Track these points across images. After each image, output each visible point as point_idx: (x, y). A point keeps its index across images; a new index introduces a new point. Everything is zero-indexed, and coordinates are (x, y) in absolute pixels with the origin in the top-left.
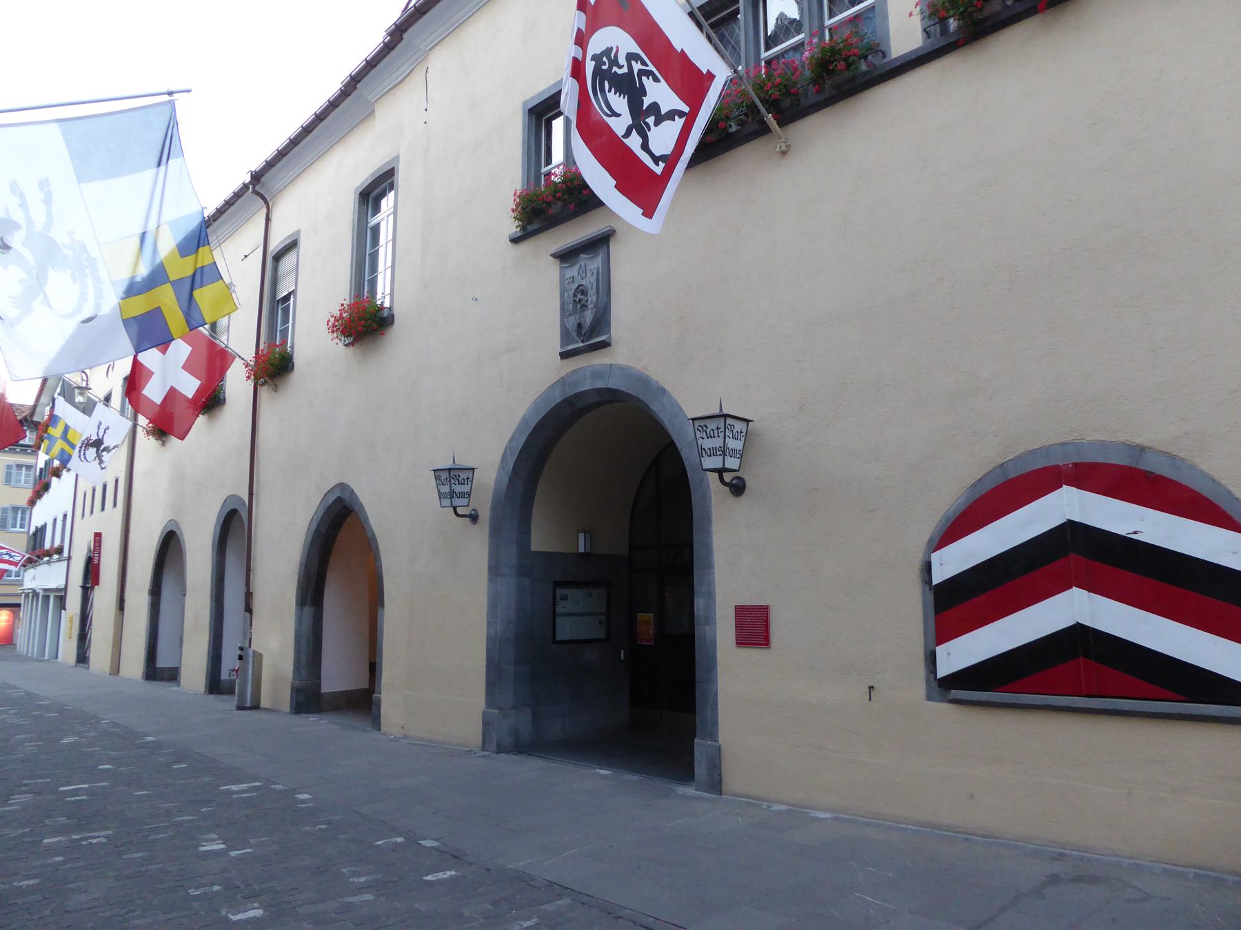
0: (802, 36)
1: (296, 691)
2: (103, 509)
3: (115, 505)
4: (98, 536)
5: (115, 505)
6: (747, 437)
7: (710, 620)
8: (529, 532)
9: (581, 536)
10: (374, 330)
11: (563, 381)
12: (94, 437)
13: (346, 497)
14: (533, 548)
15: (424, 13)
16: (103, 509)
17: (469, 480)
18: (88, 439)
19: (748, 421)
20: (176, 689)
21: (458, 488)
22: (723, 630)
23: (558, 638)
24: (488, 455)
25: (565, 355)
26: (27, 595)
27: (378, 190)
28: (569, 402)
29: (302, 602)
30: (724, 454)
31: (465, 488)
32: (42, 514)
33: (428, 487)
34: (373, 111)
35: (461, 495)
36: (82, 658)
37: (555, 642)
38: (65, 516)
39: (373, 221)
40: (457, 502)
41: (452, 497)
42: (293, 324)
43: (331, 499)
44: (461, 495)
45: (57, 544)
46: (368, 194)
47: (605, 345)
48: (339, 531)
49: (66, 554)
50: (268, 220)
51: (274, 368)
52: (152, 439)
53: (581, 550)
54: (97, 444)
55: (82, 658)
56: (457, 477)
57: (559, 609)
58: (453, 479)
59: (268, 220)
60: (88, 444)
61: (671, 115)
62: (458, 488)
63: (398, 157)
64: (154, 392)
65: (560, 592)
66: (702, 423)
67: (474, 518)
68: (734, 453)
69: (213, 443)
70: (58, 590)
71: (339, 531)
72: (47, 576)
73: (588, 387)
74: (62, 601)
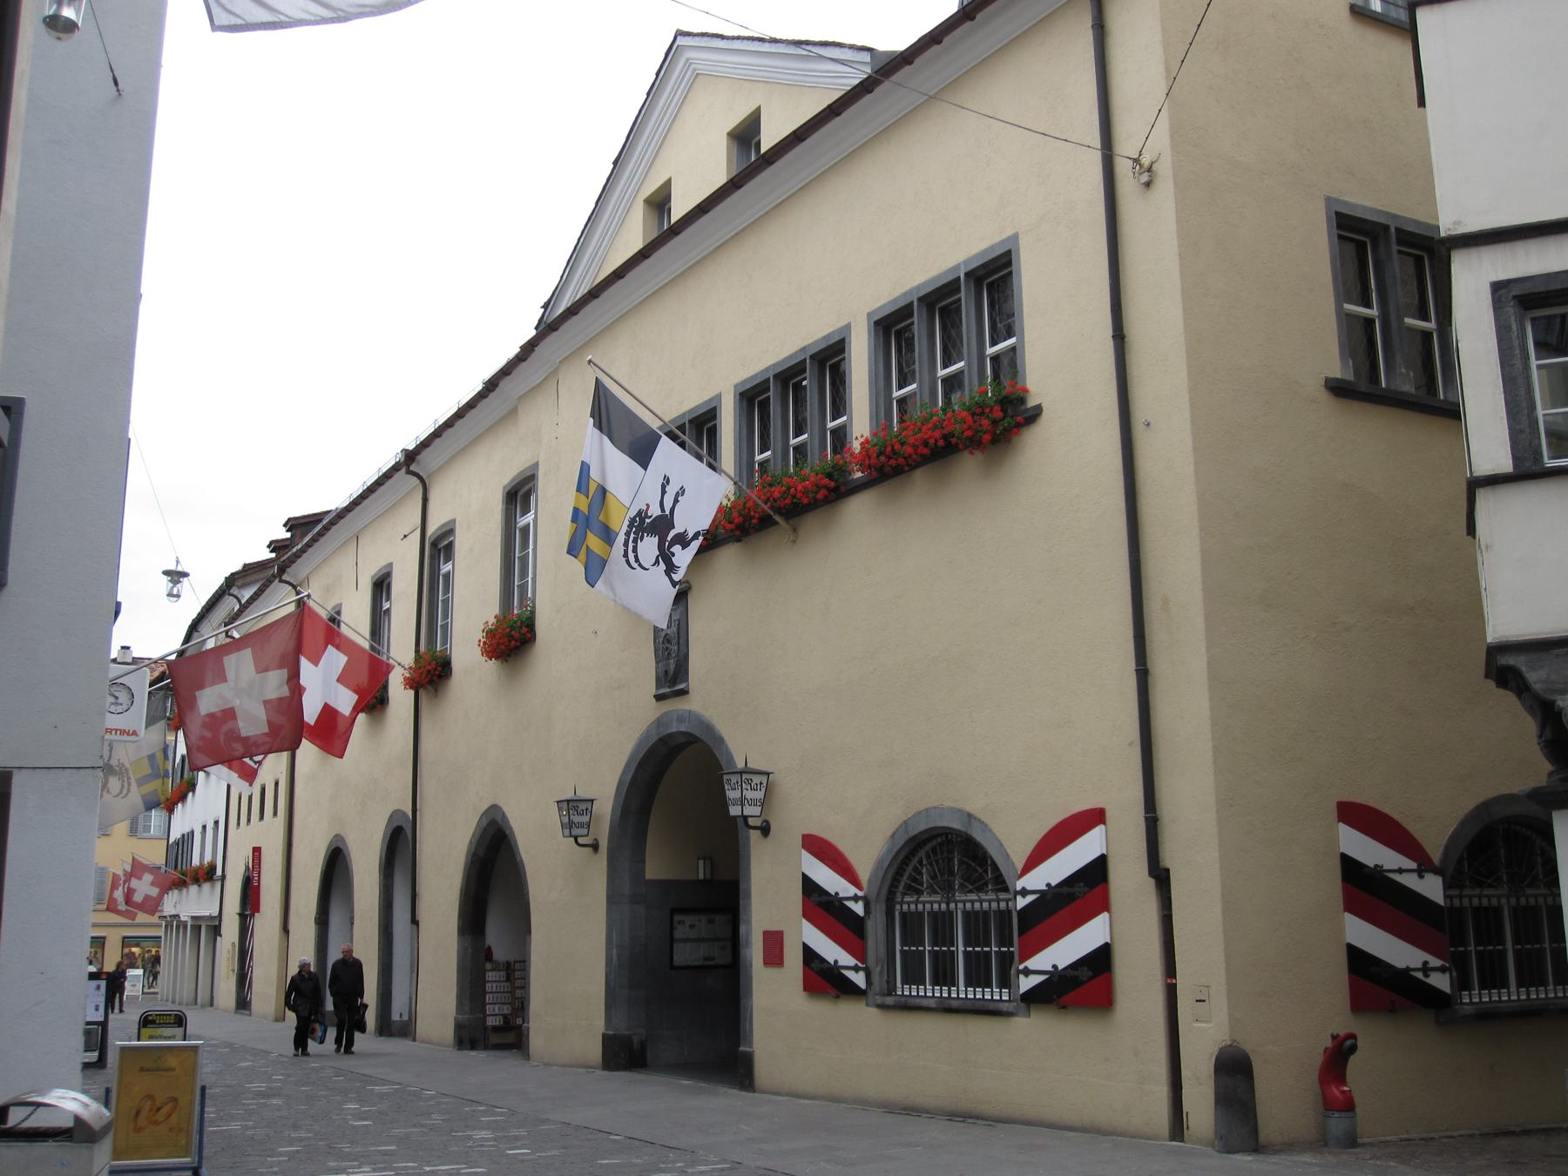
0: (962, 364)
1: (459, 1027)
2: (262, 818)
3: (275, 814)
4: (257, 851)
5: (275, 814)
6: (769, 790)
7: (748, 944)
9: (701, 863)
10: (517, 648)
11: (659, 722)
12: (655, 511)
13: (499, 819)
14: (648, 876)
15: (740, 187)
16: (262, 818)
17: (589, 811)
18: (642, 515)
19: (768, 774)
21: (576, 819)
22: (755, 952)
25: (659, 698)
26: (168, 926)
27: (526, 488)
28: (664, 741)
29: (462, 931)
30: (742, 805)
31: (585, 819)
32: (186, 819)
33: (554, 817)
35: (581, 825)
36: (243, 1004)
37: (673, 967)
38: (216, 823)
39: (522, 522)
40: (576, 832)
42: (534, 579)
43: (485, 823)
44: (581, 825)
45: (208, 858)
47: (684, 692)
48: (494, 860)
49: (219, 872)
50: (425, 500)
51: (432, 674)
53: (701, 877)
54: (661, 526)
55: (243, 1004)
57: (677, 934)
58: (574, 809)
59: (425, 500)
60: (642, 525)
62: (576, 819)
63: (537, 464)
65: (677, 918)
67: (595, 847)
68: (753, 802)
69: (377, 750)
70: (211, 918)
71: (494, 860)
72: (193, 903)
74: (216, 931)
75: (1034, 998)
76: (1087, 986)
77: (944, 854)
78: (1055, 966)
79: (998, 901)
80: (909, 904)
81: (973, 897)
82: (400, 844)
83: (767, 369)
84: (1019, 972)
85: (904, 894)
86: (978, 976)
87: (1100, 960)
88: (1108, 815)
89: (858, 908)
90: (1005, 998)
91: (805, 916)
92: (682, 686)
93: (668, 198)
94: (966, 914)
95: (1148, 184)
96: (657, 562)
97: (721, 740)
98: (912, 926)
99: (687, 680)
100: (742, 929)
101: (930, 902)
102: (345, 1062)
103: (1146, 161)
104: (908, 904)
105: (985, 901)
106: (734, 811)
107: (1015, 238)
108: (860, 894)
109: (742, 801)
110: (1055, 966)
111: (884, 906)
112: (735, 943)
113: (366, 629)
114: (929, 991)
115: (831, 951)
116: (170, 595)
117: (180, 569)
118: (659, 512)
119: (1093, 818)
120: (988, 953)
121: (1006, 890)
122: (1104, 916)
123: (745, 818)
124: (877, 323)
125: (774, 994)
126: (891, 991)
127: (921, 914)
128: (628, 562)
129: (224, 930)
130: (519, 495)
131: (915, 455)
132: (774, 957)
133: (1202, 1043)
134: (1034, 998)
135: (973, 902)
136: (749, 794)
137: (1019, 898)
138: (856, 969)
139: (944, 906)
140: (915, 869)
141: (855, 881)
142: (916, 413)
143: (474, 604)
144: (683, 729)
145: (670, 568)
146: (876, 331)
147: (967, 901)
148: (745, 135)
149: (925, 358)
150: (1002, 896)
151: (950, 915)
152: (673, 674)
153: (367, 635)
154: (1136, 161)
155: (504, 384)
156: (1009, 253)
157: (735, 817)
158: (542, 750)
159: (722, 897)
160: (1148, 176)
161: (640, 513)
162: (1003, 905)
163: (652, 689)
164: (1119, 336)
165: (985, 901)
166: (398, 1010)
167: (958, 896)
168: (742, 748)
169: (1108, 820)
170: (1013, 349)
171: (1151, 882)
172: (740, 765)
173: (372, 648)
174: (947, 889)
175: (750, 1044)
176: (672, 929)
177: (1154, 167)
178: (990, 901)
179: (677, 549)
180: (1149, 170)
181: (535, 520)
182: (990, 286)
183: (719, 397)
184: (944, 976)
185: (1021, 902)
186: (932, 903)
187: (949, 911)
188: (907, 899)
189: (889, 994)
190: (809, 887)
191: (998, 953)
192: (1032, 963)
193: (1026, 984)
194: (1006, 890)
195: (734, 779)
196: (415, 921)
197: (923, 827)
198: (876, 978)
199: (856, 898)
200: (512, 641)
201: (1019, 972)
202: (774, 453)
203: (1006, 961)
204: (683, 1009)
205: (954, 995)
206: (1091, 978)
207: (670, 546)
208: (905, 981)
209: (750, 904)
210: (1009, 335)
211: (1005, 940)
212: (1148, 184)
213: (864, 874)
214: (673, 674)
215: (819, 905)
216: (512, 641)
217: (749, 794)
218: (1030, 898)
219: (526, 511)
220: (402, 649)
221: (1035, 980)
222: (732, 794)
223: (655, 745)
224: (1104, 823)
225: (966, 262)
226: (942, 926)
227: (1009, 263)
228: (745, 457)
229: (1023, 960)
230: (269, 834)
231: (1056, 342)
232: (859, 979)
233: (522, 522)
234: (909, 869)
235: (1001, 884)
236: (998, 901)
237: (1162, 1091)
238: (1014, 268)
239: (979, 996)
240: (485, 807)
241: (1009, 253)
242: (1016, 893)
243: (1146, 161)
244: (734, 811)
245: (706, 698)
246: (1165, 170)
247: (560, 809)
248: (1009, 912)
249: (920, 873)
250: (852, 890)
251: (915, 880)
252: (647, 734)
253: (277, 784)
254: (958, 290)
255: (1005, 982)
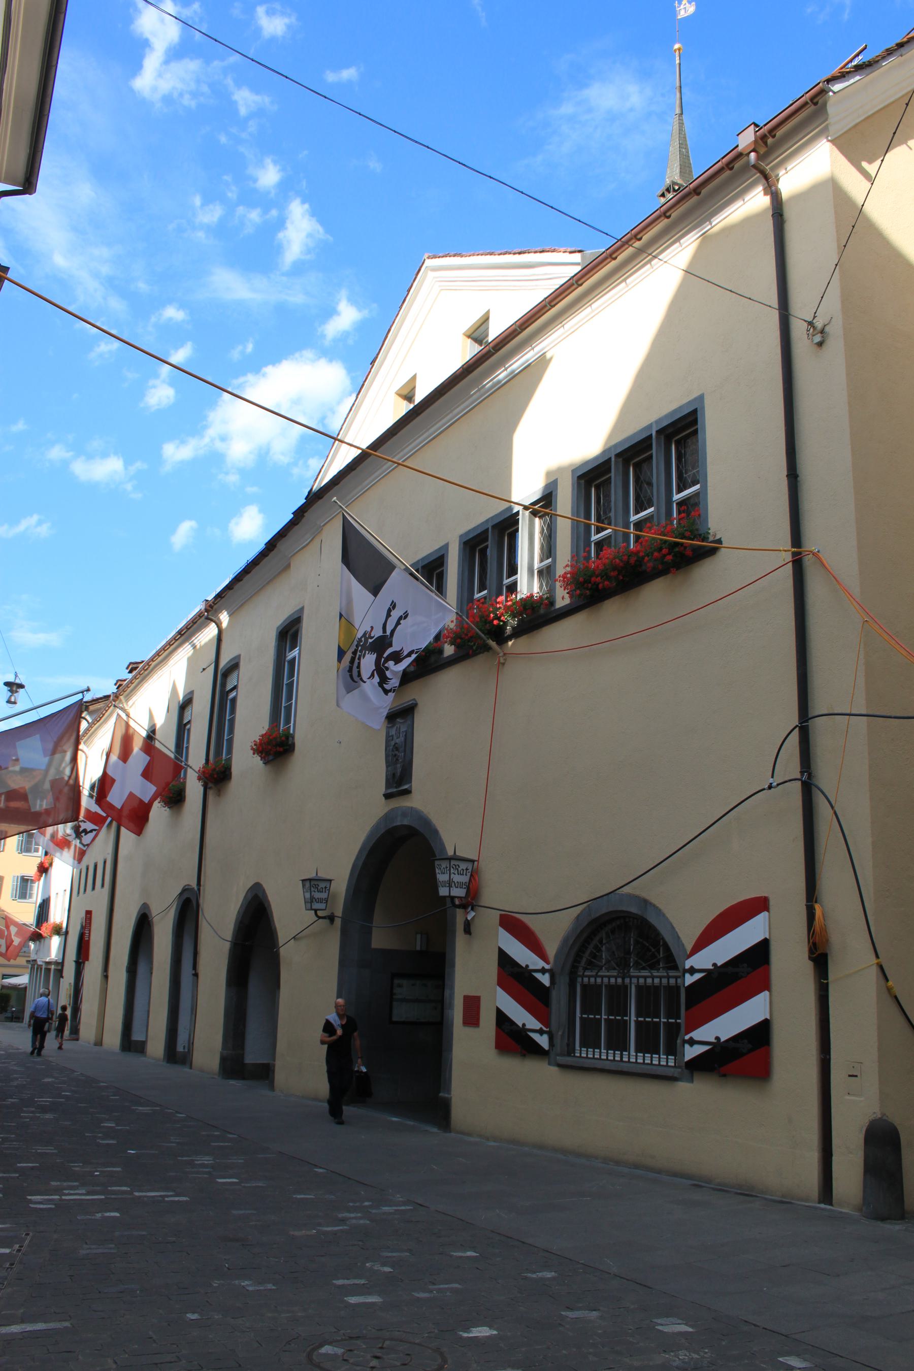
0: (652, 509)
1: (223, 1060)
2: (94, 888)
3: (103, 885)
4: (89, 913)
5: (103, 885)
6: (474, 875)
7: (451, 1006)
8: (371, 933)
9: (419, 936)
11: (387, 817)
12: (377, 633)
13: (260, 895)
16: (94, 888)
20: (187, 1070)
21: (317, 895)
22: (457, 1014)
23: (395, 1019)
24: (340, 872)
30: (450, 886)
34: (288, 567)
35: (320, 901)
41: (450, 886)
44: (320, 901)
46: (287, 632)
47: (408, 792)
51: (217, 777)
52: (257, 759)
53: (418, 948)
56: (316, 886)
58: (314, 885)
61: (91, 831)
62: (317, 895)
64: (116, 798)
65: (396, 981)
66: (316, 883)
67: (331, 918)
70: (56, 963)
71: (256, 924)
73: (399, 824)
74: (60, 973)
75: (698, 1066)
76: (746, 1057)
77: (621, 934)
78: (717, 1038)
79: (668, 977)
80: (589, 977)
81: (645, 973)
82: (188, 909)
83: (487, 521)
84: (685, 1042)
85: (585, 969)
86: (647, 1044)
87: (759, 1035)
88: (772, 903)
89: (545, 979)
90: (671, 1063)
91: (500, 984)
92: (406, 787)
93: (414, 395)
94: (639, 987)
95: (820, 344)
96: (372, 675)
97: (436, 832)
98: (591, 996)
99: (410, 782)
100: (447, 993)
101: (608, 977)
102: (39, 1059)
103: (819, 324)
104: (588, 977)
105: (656, 978)
106: (443, 892)
107: (701, 398)
108: (547, 967)
109: (450, 884)
110: (717, 1038)
111: (567, 979)
112: (441, 1004)
113: (172, 745)
114: (604, 1055)
115: (521, 1016)
116: (9, 702)
117: (18, 681)
118: (381, 633)
119: (757, 906)
120: (658, 1023)
121: (675, 968)
122: (766, 994)
123: (453, 898)
124: (579, 478)
125: (471, 1051)
126: (570, 1051)
127: (600, 986)
128: (351, 676)
129: (64, 974)
130: (289, 634)
131: (603, 583)
132: (472, 1017)
133: (853, 1115)
134: (698, 1066)
135: (645, 978)
136: (457, 878)
137: (687, 976)
138: (541, 1032)
139: (620, 980)
140: (596, 947)
141: (542, 955)
142: (609, 552)
143: (252, 720)
144: (406, 822)
145: (383, 680)
146: (579, 484)
147: (642, 976)
148: (477, 334)
149: (620, 504)
150: (672, 973)
151: (625, 989)
152: (399, 779)
153: (173, 749)
154: (810, 324)
155: (281, 546)
156: (695, 412)
157: (445, 897)
158: (299, 838)
159: (431, 966)
160: (821, 341)
161: (365, 634)
162: (672, 981)
163: (382, 789)
164: (793, 475)
165: (656, 978)
166: (137, 1036)
167: (633, 972)
168: (456, 837)
169: (771, 908)
170: (697, 494)
171: (809, 965)
172: (450, 853)
173: (176, 757)
174: (623, 966)
175: (449, 1091)
176: (392, 988)
177: (827, 329)
178: (661, 978)
179: (391, 664)
180: (822, 332)
181: (300, 654)
182: (678, 443)
183: (446, 547)
184: (618, 1042)
185: (689, 980)
186: (609, 977)
187: (624, 983)
188: (587, 973)
189: (569, 1054)
190: (504, 959)
191: (667, 1024)
192: (696, 1035)
193: (691, 1052)
194: (675, 968)
195: (444, 864)
196: (196, 975)
197: (604, 911)
198: (557, 1041)
199: (543, 971)
200: (277, 748)
201: (685, 1042)
202: (489, 592)
203: (673, 1033)
204: (391, 1054)
205: (625, 1059)
206: (750, 1051)
207: (387, 660)
208: (584, 1044)
209: (454, 972)
210: (694, 483)
211: (673, 1012)
212: (820, 344)
213: (552, 950)
214: (399, 779)
215: (512, 976)
216: (277, 748)
217: (457, 878)
218: (697, 976)
219: (293, 647)
220: (197, 757)
221: (699, 1050)
222: (442, 877)
223: (383, 836)
224: (768, 911)
225: (657, 422)
226: (618, 997)
227: (695, 422)
228: (466, 594)
229: (687, 1033)
230: (98, 901)
231: (736, 483)
232: (543, 1041)
233: (290, 656)
234: (591, 948)
235: (672, 963)
236: (668, 977)
237: (813, 1157)
238: (699, 426)
239: (648, 1061)
240: (250, 884)
241: (695, 412)
242: (685, 971)
243: (819, 324)
244: (443, 892)
245: (423, 798)
246: (836, 331)
247: (304, 886)
248: (677, 988)
249: (600, 950)
250: (541, 964)
251: (595, 957)
252: (376, 827)
253: (105, 862)
254: (650, 447)
255: (672, 1050)
